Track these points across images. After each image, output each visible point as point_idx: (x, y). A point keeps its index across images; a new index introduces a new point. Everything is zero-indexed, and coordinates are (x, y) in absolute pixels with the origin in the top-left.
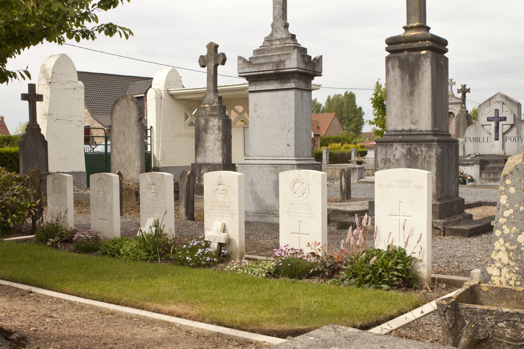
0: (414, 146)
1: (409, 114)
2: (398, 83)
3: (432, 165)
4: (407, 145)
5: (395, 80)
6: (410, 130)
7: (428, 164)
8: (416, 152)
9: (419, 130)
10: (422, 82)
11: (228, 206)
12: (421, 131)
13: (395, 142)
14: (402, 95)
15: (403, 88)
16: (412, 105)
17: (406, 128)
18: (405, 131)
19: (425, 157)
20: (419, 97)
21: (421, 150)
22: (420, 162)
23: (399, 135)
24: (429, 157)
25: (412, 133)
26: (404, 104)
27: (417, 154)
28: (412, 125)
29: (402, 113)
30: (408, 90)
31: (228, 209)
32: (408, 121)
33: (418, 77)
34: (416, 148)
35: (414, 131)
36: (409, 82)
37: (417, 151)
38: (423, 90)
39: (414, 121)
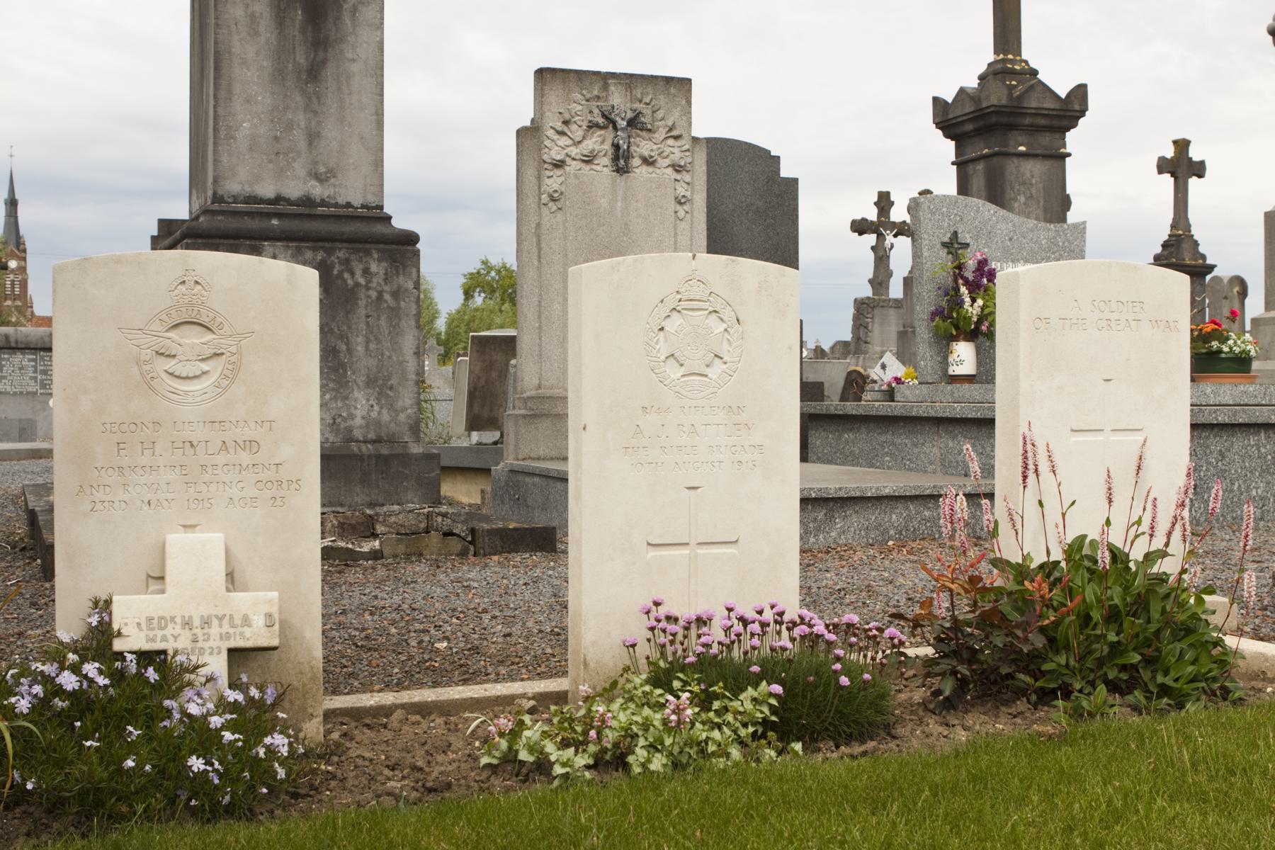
0: (341, 254)
1: (302, 144)
2: (262, 29)
3: (403, 323)
4: (315, 249)
5: (253, 18)
6: (307, 201)
7: (390, 319)
8: (346, 275)
9: (341, 201)
10: (351, 39)
11: (251, 445)
12: (349, 205)
13: (267, 239)
14: (278, 74)
15: (281, 52)
16: (315, 113)
17: (294, 190)
18: (289, 202)
19: (380, 294)
20: (339, 89)
21: (366, 271)
22: (362, 312)
23: (270, 215)
24: (396, 294)
25: (313, 211)
26: (286, 108)
27: (350, 282)
28: (314, 182)
29: (276, 139)
30: (301, 58)
31: (245, 458)
32: (300, 168)
33: (338, 18)
34: (346, 262)
35: (323, 203)
36: (303, 31)
37: (353, 274)
38: (355, 68)
39: (322, 169)
